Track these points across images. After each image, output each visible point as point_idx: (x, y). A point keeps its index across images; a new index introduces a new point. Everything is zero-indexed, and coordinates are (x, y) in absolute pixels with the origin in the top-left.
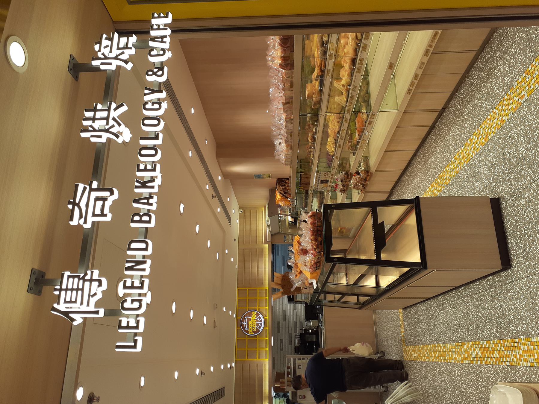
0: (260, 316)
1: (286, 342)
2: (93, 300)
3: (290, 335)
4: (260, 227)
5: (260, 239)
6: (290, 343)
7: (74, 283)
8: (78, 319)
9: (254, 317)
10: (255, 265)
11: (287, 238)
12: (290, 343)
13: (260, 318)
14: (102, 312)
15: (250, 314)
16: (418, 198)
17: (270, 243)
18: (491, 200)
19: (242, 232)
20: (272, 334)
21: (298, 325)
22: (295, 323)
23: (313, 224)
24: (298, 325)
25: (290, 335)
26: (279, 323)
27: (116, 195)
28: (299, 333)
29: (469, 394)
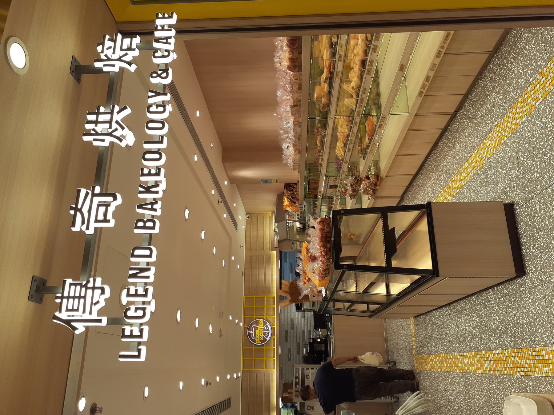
0: (268, 324)
1: (294, 351)
2: (96, 309)
3: (298, 344)
4: (267, 233)
5: (267, 245)
6: (298, 353)
7: (76, 291)
8: (80, 328)
9: (261, 326)
10: (262, 272)
11: (295, 244)
12: (298, 353)
13: (267, 326)
14: (105, 320)
15: (257, 323)
16: (429, 203)
17: (278, 249)
18: (505, 205)
19: (249, 238)
20: (280, 343)
21: (306, 334)
22: (304, 332)
23: (322, 230)
24: (306, 334)
25: (298, 344)
26: (286, 332)
27: (119, 201)
28: (307, 342)
29: (482, 404)
